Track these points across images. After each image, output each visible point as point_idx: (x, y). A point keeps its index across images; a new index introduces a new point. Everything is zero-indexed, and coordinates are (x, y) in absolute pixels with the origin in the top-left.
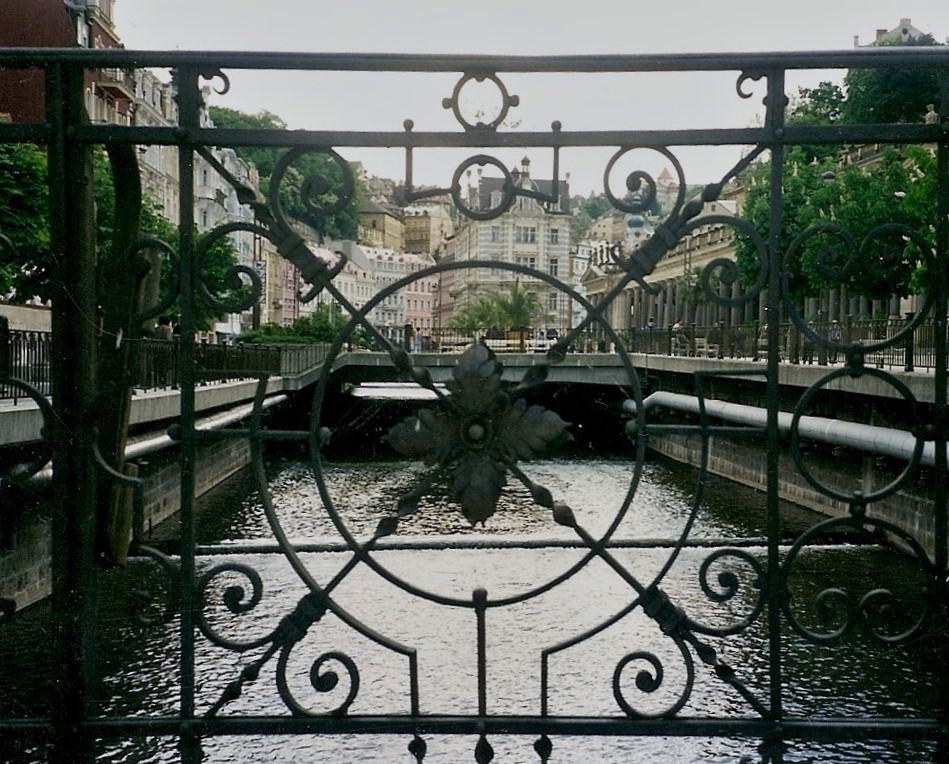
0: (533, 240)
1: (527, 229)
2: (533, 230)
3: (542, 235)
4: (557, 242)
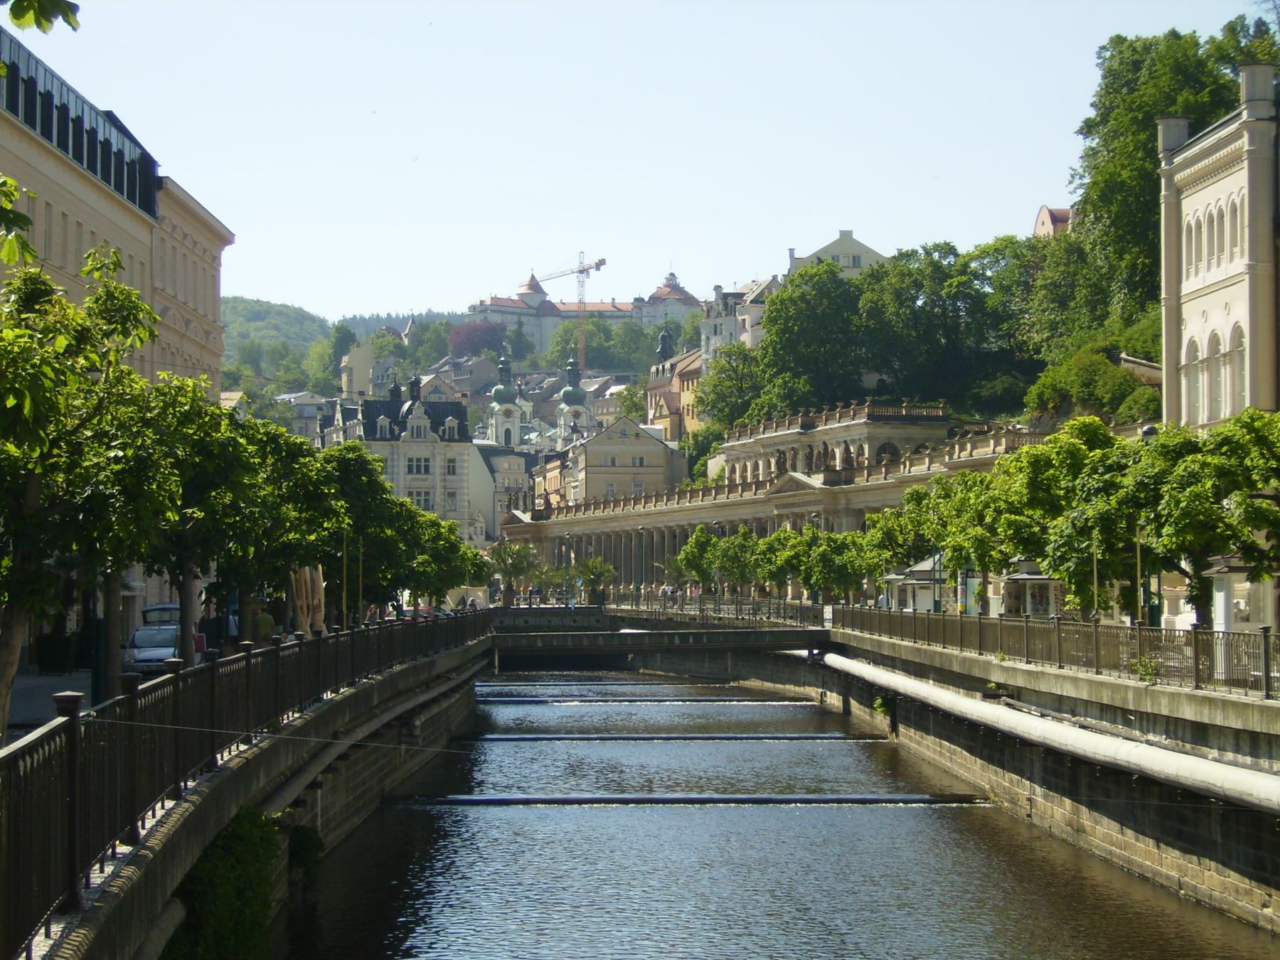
0: (427, 471)
1: (419, 460)
2: (427, 460)
3: (438, 466)
4: (454, 473)
